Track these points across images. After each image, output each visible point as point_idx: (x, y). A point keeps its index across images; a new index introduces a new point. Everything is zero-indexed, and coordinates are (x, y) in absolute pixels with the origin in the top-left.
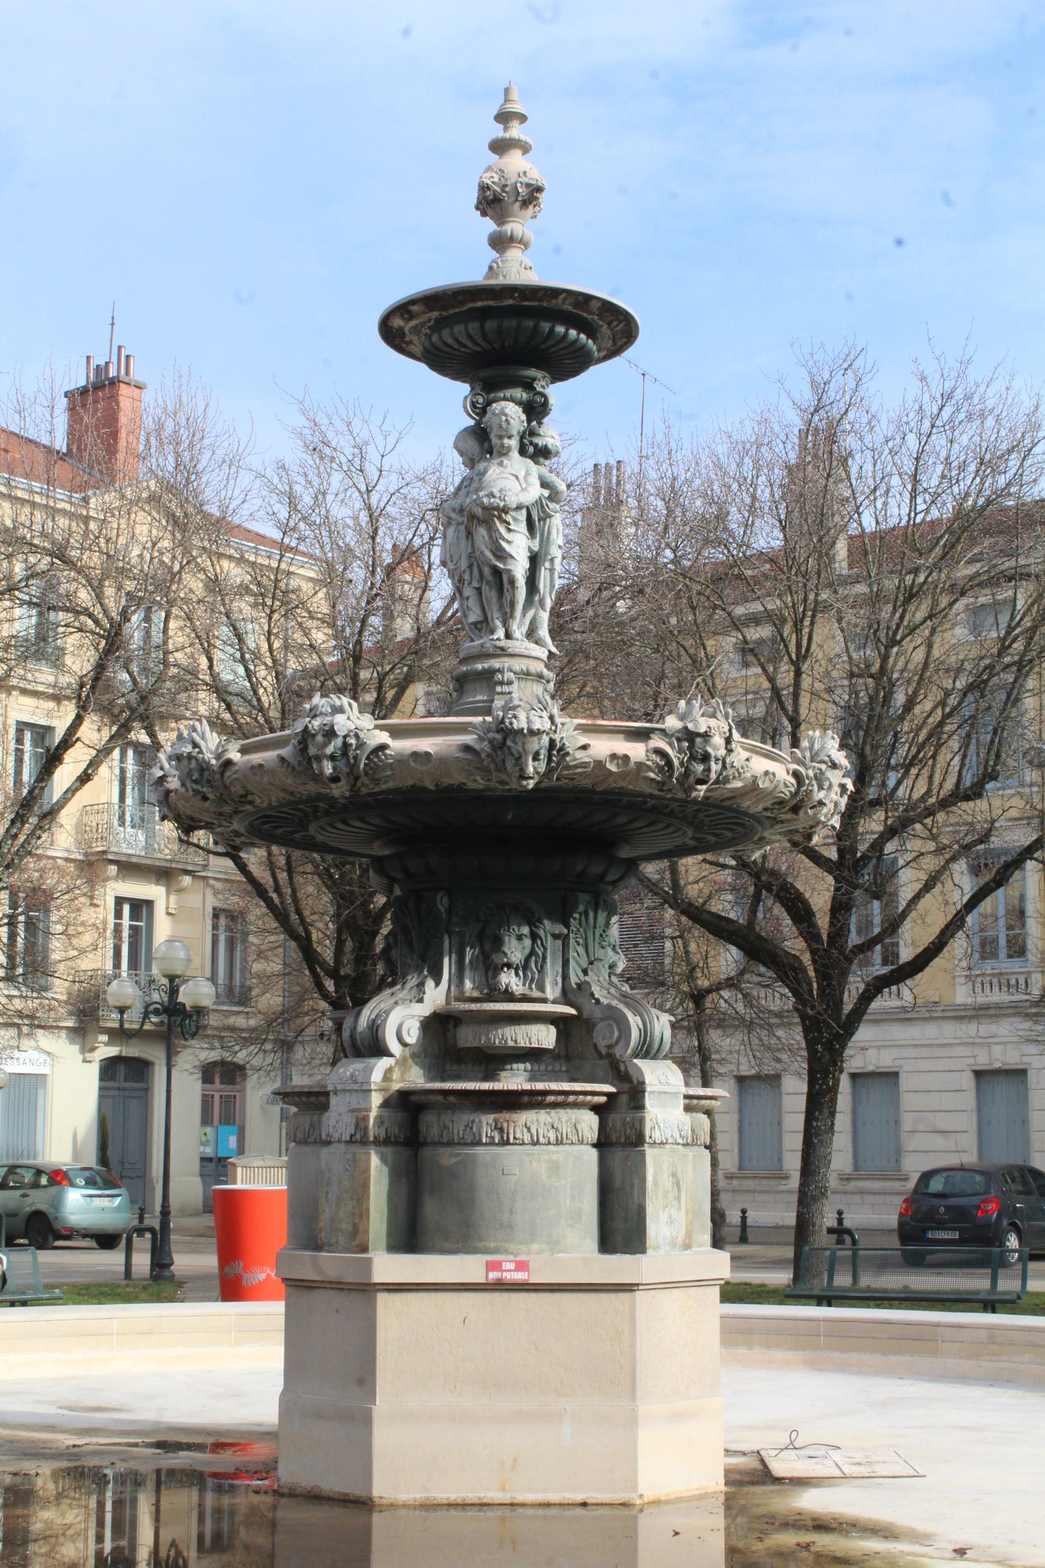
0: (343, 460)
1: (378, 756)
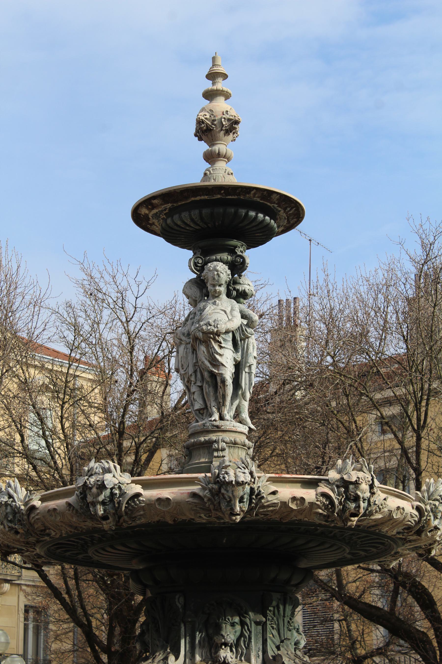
0: (110, 301)
1: (134, 502)
